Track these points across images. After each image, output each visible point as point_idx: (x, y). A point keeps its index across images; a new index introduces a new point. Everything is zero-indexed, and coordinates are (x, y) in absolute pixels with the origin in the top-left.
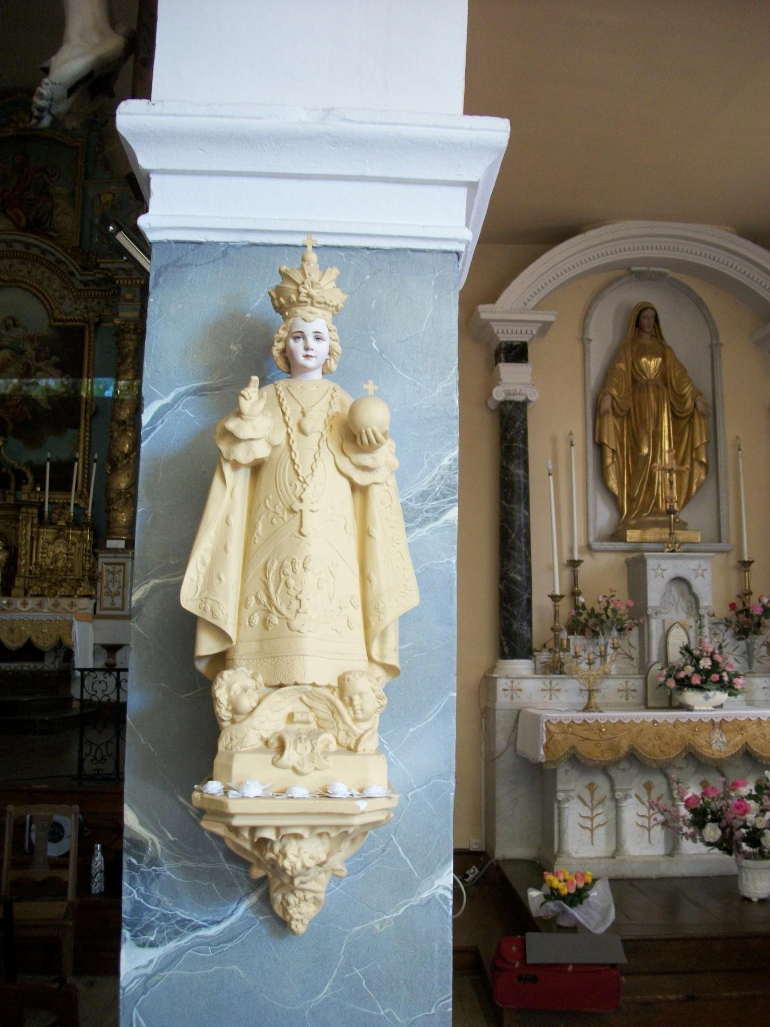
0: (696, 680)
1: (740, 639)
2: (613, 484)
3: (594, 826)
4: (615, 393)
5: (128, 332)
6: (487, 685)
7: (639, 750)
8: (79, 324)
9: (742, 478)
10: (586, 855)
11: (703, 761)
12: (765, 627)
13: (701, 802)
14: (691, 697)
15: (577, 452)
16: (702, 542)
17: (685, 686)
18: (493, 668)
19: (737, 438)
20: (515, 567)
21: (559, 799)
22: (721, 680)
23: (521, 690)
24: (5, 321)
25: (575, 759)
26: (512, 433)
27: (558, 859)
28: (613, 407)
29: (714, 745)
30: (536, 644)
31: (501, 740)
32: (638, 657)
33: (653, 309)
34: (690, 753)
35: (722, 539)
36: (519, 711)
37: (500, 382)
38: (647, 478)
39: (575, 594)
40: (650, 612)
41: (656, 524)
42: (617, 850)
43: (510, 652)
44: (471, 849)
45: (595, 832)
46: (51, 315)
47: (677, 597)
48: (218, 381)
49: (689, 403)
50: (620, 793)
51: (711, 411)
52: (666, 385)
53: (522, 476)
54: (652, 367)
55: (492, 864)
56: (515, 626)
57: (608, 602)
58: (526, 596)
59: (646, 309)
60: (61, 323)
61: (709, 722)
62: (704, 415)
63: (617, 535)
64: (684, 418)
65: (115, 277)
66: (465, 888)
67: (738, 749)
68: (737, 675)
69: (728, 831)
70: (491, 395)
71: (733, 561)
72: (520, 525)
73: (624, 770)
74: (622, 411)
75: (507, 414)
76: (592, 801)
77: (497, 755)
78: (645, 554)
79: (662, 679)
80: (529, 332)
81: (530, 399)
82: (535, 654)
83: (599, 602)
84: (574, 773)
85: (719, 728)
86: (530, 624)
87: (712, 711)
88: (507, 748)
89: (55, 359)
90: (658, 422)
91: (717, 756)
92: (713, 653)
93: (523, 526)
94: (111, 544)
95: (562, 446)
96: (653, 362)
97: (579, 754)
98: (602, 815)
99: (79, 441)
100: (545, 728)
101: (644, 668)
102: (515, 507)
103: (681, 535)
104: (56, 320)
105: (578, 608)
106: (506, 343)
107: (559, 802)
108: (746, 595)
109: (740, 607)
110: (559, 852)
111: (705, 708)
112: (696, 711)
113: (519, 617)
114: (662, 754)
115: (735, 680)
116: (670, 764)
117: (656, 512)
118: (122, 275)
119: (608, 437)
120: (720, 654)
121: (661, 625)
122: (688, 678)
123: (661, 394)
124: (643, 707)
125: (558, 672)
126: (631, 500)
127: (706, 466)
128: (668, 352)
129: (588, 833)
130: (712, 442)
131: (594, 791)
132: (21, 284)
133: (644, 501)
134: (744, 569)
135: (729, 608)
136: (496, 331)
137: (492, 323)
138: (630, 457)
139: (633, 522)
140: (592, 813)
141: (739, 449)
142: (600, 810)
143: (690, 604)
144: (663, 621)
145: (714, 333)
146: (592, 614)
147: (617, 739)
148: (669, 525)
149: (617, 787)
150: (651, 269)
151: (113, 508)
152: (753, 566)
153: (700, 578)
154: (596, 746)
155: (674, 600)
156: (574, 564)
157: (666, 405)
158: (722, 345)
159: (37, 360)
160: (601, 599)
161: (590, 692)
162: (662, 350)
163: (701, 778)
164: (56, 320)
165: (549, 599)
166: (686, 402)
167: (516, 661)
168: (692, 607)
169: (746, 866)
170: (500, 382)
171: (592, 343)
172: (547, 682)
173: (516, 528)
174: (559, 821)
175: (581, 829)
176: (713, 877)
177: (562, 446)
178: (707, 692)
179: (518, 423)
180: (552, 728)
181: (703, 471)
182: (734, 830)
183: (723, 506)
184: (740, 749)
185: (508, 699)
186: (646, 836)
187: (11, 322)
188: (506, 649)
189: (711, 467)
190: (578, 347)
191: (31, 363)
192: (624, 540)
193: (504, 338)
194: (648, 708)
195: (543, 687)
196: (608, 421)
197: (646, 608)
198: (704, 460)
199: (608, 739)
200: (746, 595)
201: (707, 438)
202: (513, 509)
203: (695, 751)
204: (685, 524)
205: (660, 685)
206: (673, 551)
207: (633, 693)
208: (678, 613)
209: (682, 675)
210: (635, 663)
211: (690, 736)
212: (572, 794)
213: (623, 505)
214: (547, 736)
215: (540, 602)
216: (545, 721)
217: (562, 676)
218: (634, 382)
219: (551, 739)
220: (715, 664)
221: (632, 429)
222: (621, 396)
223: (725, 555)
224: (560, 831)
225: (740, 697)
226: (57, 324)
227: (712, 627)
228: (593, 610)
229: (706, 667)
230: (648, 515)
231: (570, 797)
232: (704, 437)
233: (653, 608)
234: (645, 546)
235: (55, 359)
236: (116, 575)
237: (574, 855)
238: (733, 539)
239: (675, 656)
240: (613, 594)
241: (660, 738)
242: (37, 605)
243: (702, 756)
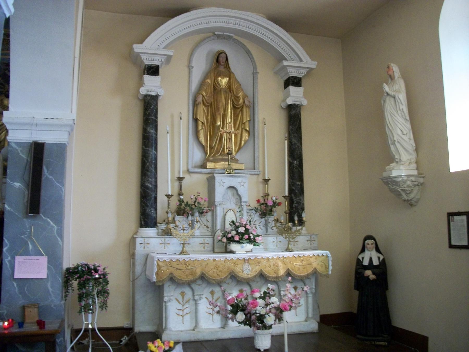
0: (237, 238)
1: (261, 218)
2: (202, 138)
3: (184, 314)
4: (204, 94)
6: (133, 241)
7: (206, 274)
9: (265, 138)
10: (180, 329)
11: (239, 280)
12: (274, 212)
13: (236, 301)
14: (234, 247)
15: (184, 123)
16: (245, 169)
17: (231, 241)
18: (136, 233)
19: (264, 118)
20: (148, 180)
21: (165, 300)
22: (249, 238)
23: (149, 244)
25: (172, 279)
26: (149, 111)
27: (164, 332)
28: (203, 101)
29: (245, 272)
30: (159, 219)
31: (138, 268)
32: (211, 227)
33: (225, 54)
34: (233, 275)
35: (256, 168)
36: (148, 255)
37: (144, 85)
38: (219, 137)
39: (180, 194)
40: (216, 203)
41: (223, 160)
42: (196, 326)
43: (145, 224)
44: (125, 327)
45: (185, 317)
47: (231, 196)
49: (241, 101)
50: (197, 297)
51: (252, 105)
52: (230, 92)
53: (153, 134)
54: (224, 82)
55: (133, 334)
56: (147, 211)
57: (196, 198)
58: (154, 195)
59: (221, 53)
61: (242, 260)
62: (248, 107)
63: (204, 166)
64: (238, 108)
66: (112, 349)
67: (257, 273)
68: (258, 236)
69: (249, 315)
70: (139, 92)
71: (261, 180)
72: (152, 158)
73: (199, 285)
74: (208, 103)
75: (147, 102)
76: (183, 301)
77: (136, 278)
78: (214, 174)
79: (220, 238)
80: (160, 60)
81: (159, 94)
82: (158, 225)
83: (192, 199)
84: (173, 287)
85: (247, 262)
86: (156, 209)
87: (245, 254)
88: (141, 274)
90: (225, 110)
91: (246, 276)
92: (246, 225)
93: (153, 159)
95: (176, 119)
96: (224, 80)
97: (174, 277)
98: (189, 307)
100: (156, 264)
101: (213, 233)
102: (150, 149)
103: (234, 166)
105: (181, 201)
106: (148, 65)
107: (165, 302)
108: (266, 196)
109: (262, 201)
110: (165, 328)
111: (242, 253)
112: (237, 254)
113: (150, 206)
114: (218, 276)
115: (257, 238)
116: (222, 281)
117: (223, 153)
119: (200, 115)
120: (250, 225)
121: (222, 210)
122: (233, 237)
123: (228, 96)
124: (212, 252)
125: (170, 234)
126: (211, 148)
127: (248, 132)
128: (232, 75)
129: (181, 317)
130: (252, 121)
131: (184, 296)
133: (217, 149)
134: (265, 183)
135: (256, 202)
136: (143, 59)
137: (141, 54)
138: (211, 127)
139: (211, 159)
140: (183, 308)
141: (265, 124)
142: (187, 306)
143: (237, 200)
144: (224, 209)
145: (255, 67)
146: (187, 204)
147: (195, 269)
148: (228, 160)
149: (196, 294)
150: (225, 34)
152: (270, 181)
153: (242, 187)
154: (183, 272)
155: (229, 198)
156: (180, 179)
157: (230, 101)
158: (258, 73)
160: (192, 197)
161: (184, 244)
162: (229, 74)
163: (239, 288)
165: (166, 197)
166: (240, 100)
167: (148, 228)
168: (238, 201)
169: (257, 333)
170: (144, 85)
171: (193, 68)
172: (163, 239)
173: (150, 160)
174: (166, 312)
175: (177, 316)
176: (245, 338)
177: (176, 119)
178: (243, 244)
179: (153, 106)
180: (160, 263)
181: (247, 134)
182: (251, 315)
183: (256, 153)
184: (258, 273)
185: (142, 249)
186: (211, 318)
188: (143, 223)
189: (251, 133)
190: (187, 69)
192: (206, 168)
193: (147, 62)
194: (214, 252)
195: (161, 242)
196: (200, 108)
197: (215, 202)
198: (248, 129)
199: (191, 269)
200: (266, 196)
201: (249, 119)
202: (148, 150)
203: (235, 274)
204: (238, 160)
205: (219, 241)
206: (230, 173)
207: (207, 245)
208: (231, 204)
209: (230, 235)
210: (209, 229)
211: (233, 267)
212: (172, 298)
213: (207, 150)
214: (157, 268)
215: (161, 199)
216: (156, 260)
217: (170, 236)
218: (215, 89)
219: (160, 269)
220: (247, 230)
221: (213, 113)
222: (208, 95)
223: (257, 176)
224: (166, 317)
225: (261, 246)
227: (249, 211)
228: (187, 202)
229: (242, 231)
230: (219, 156)
231: (171, 299)
232: (248, 118)
233: (218, 202)
234: (217, 171)
237: (173, 329)
238: (261, 169)
239: (228, 227)
240: (199, 194)
241: (217, 268)
243: (239, 277)
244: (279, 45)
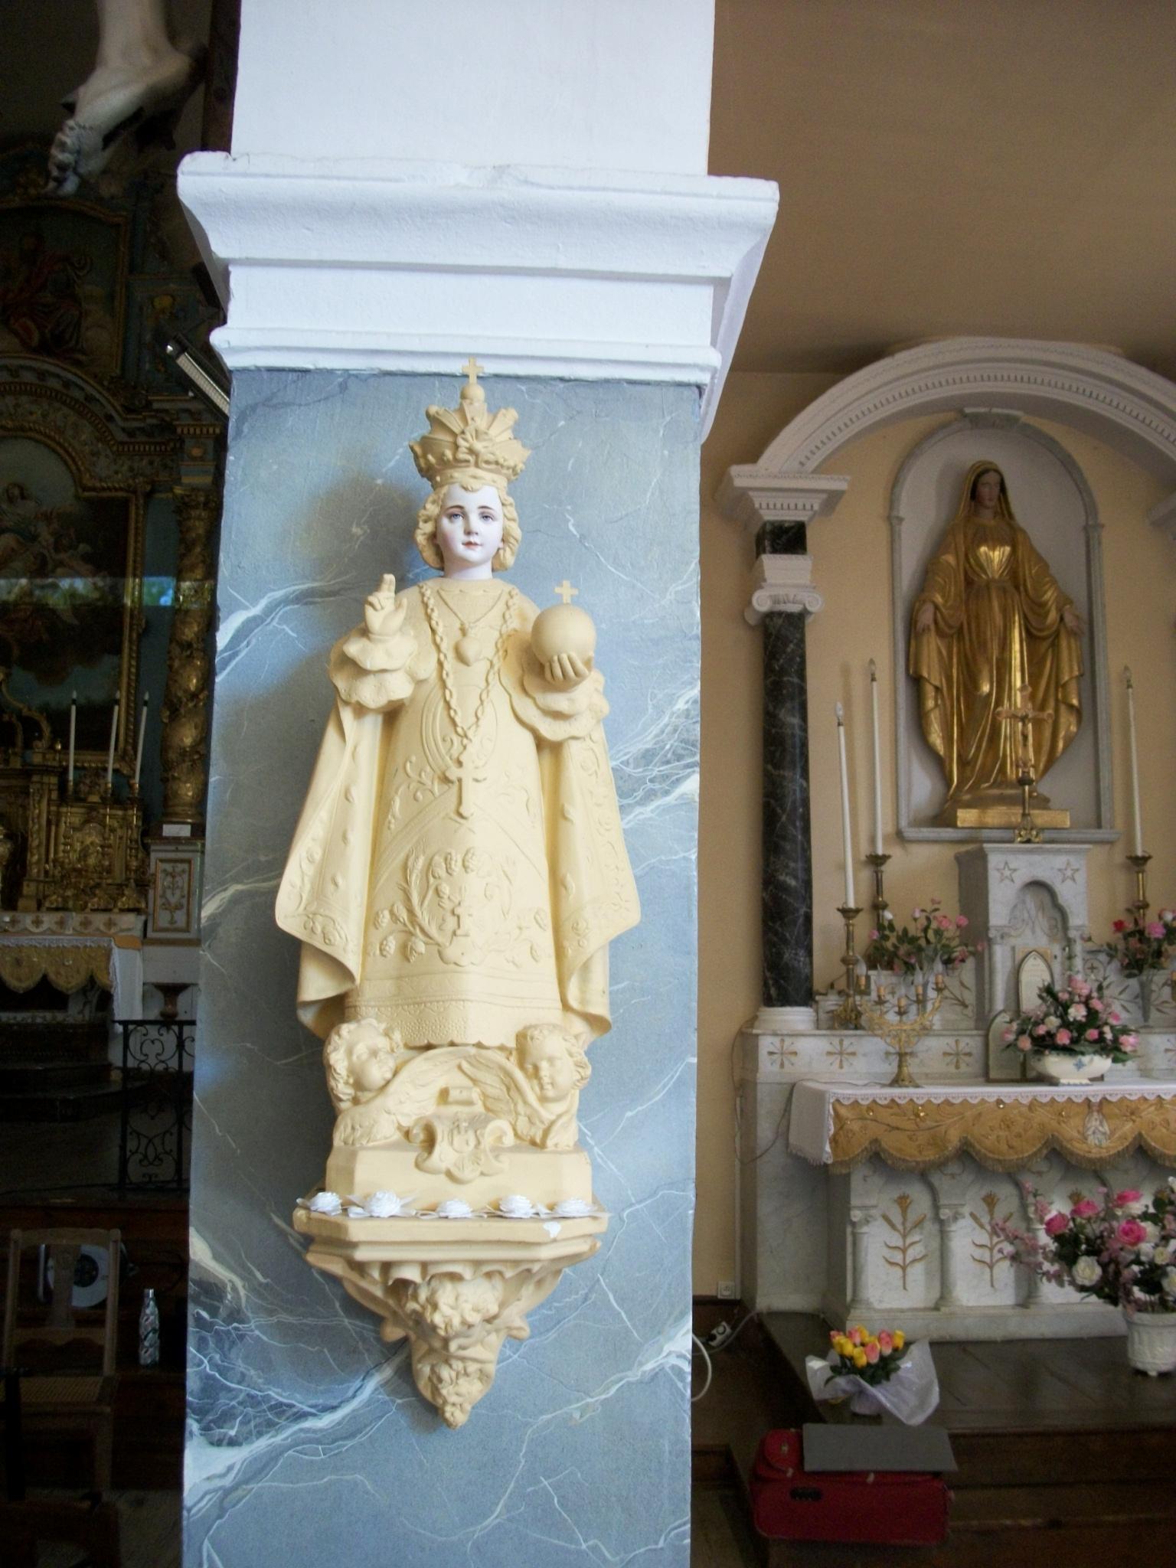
0: (1063, 1038)
1: (1130, 976)
2: (936, 739)
3: (908, 1260)
4: (939, 599)
5: (196, 507)
6: (744, 1045)
7: (976, 1145)
8: (120, 494)
9: (1133, 729)
10: (895, 1305)
11: (1074, 1162)
12: (1168, 957)
13: (1071, 1224)
14: (1055, 1064)
15: (881, 691)
16: (1071, 827)
17: (1046, 1047)
18: (753, 1020)
19: (1126, 668)
20: (787, 866)
21: (854, 1219)
22: (1101, 1038)
23: (795, 1053)
24: (7, 491)
25: (878, 1159)
26: (781, 661)
27: (852, 1311)
28: (936, 622)
29: (1091, 1138)
30: (818, 984)
31: (765, 1130)
32: (974, 1003)
33: (997, 471)
34: (1054, 1150)
35: (1103, 823)
36: (793, 1086)
37: (763, 584)
38: (988, 731)
39: (878, 907)
40: (992, 934)
41: (1002, 800)
42: (942, 1297)
43: (778, 995)
44: (719, 1297)
45: (909, 1270)
46: (78, 482)
47: (1033, 912)
48: (332, 582)
49: (1053, 616)
50: (947, 1211)
51: (1085, 627)
52: (1017, 588)
53: (796, 727)
54: (996, 560)
55: (752, 1319)
56: (786, 956)
57: (928, 919)
58: (803, 910)
59: (986, 471)
60: (93, 494)
61: (1084, 1102)
62: (1075, 634)
63: (942, 817)
64: (1044, 639)
65: (175, 423)
66: (710, 1356)
67: (1126, 1144)
68: (1125, 1031)
69: (1112, 1268)
70: (750, 602)
71: (1119, 857)
72: (794, 802)
73: (953, 1176)
74: (950, 627)
75: (774, 632)
76: (903, 1224)
77: (758, 1153)
78: (985, 845)
79: (1011, 1037)
80: (808, 507)
81: (809, 608)
82: (817, 998)
83: (915, 920)
84: (877, 1181)
85: (1098, 1111)
86: (809, 952)
87: (1087, 1085)
88: (774, 1142)
89: (83, 547)
90: (1005, 645)
91: (1095, 1154)
92: (1089, 997)
93: (798, 803)
94: (169, 830)
95: (858, 681)
96: (997, 553)
97: (884, 1151)
98: (920, 1244)
99: (120, 673)
100: (832, 1112)
101: (983, 1020)
102: (787, 773)
103: (1040, 817)
104: (85, 489)
105: (883, 928)
106: (772, 523)
107: (854, 1224)
108: (1139, 908)
109: (1130, 926)
110: (853, 1300)
111: (1077, 1082)
112: (1064, 1085)
113: (793, 942)
114: (1011, 1151)
115: (1123, 1038)
116: (1024, 1167)
117: (1002, 782)
118: (186, 420)
119: (929, 667)
120: (1100, 998)
121: (1009, 954)
122: (1050, 1035)
123: (1009, 601)
124: (982, 1079)
125: (852, 1026)
126: (963, 763)
127: (1078, 712)
128: (1020, 538)
129: (898, 1271)
130: (1088, 675)
131: (907, 1207)
132: (32, 434)
133: (983, 765)
134: (1136, 869)
135: (1113, 928)
136: (757, 506)
137: (751, 493)
138: (962, 698)
139: (967, 797)
140: (904, 1241)
141: (1129, 686)
142: (916, 1237)
143: (1054, 922)
144: (1013, 949)
145: (1090, 509)
146: (905, 937)
147: (943, 1129)
148: (1021, 801)
149: (943, 1201)
150: (995, 410)
151: (173, 776)
152: (1150, 863)
153: (1069, 882)
154: (911, 1139)
155: (1030, 917)
156: (876, 861)
157: (1017, 618)
158: (1103, 526)
159: (57, 550)
160: (917, 914)
161: (901, 1056)
162: (1011, 534)
163: (1070, 1187)
164: (85, 489)
165: (839, 915)
166: (1047, 613)
167: (788, 1009)
168: (1056, 926)
169: (1139, 1322)
170: (763, 584)
171: (904, 523)
172: (836, 1041)
173: (789, 806)
174: (854, 1254)
175: (887, 1266)
176: (1089, 1338)
177: (858, 681)
178: (1080, 1057)
179: (792, 646)
180: (843, 1112)
181: (1073, 719)
182: (1121, 1267)
183: (1104, 773)
184: (1131, 1144)
185: (776, 1068)
186: (987, 1276)
187: (16, 492)
188: (773, 991)
189: (1086, 714)
190: (883, 530)
191: (47, 555)
192: (952, 824)
193: (769, 516)
194: (989, 1081)
195: (830, 1048)
196: (928, 642)
197: (987, 929)
198: (1075, 702)
199: (929, 1129)
200: (1139, 908)
201: (1079, 669)
202: (784, 777)
203: (1062, 1146)
204: (1047, 800)
205: (1009, 1046)
206: (1029, 841)
207: (967, 1059)
208: (1036, 936)
209: (1041, 1030)
210: (969, 1012)
211: (1054, 1124)
212: (873, 1212)
213: (951, 772)
214: (835, 1124)
215: (825, 918)
216: (832, 1101)
217: (858, 1032)
218: (969, 583)
219: (841, 1128)
220: (1092, 1014)
221: (966, 656)
222: (949, 604)
223: (1107, 847)
224: (855, 1269)
225: (1130, 1064)
226: (86, 494)
227: (1088, 957)
228: (905, 931)
229: (1079, 1018)
230: (990, 787)
231: (871, 1216)
232: (1076, 668)
233: (998, 928)
234: (986, 834)
235: (83, 547)
236: (178, 879)
237: (877, 1305)
238: (1119, 823)
239: (1031, 1001)
240: (936, 906)
241: (1008, 1127)
242: (56, 923)
243: (1072, 1154)
244: (1136, 417)
